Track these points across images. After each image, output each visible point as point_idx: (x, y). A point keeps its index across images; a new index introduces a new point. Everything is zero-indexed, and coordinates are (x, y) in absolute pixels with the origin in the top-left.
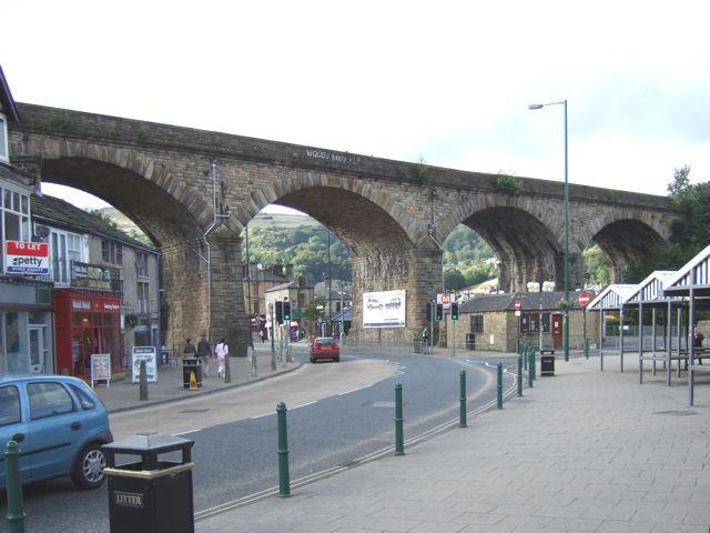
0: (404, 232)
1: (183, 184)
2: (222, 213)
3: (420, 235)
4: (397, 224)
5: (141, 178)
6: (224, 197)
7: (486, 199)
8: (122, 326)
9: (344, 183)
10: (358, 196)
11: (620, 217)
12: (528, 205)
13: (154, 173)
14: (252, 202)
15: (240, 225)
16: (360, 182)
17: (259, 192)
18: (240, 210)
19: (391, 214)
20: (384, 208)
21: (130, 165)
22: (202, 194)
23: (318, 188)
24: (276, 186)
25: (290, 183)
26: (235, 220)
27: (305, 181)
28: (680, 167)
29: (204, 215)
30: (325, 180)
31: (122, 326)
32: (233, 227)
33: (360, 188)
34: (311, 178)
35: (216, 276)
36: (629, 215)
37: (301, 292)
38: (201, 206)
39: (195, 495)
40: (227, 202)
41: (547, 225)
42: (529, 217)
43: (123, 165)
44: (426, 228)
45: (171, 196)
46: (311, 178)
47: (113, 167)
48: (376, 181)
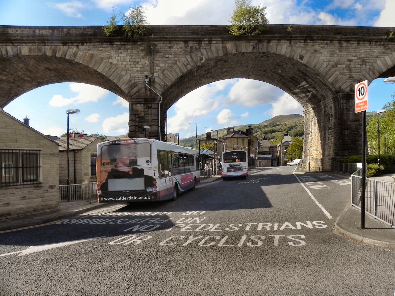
7: (225, 48)
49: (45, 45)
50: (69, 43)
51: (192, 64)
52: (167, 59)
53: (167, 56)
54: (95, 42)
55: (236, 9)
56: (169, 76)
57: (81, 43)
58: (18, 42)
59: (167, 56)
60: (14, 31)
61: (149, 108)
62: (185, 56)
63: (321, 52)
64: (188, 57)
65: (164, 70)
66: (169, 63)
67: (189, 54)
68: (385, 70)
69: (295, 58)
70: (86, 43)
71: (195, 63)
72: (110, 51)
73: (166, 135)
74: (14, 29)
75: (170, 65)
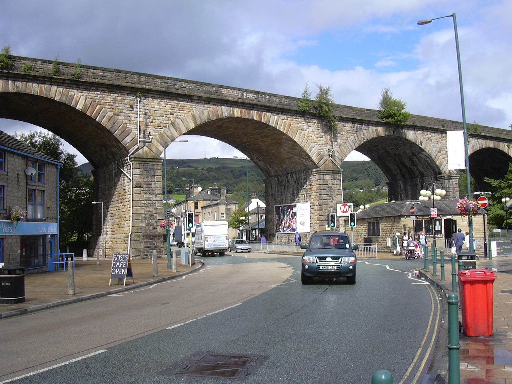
0: (307, 155)
1: (110, 114)
2: (144, 138)
3: (321, 157)
4: (301, 148)
5: (74, 109)
6: (147, 125)
7: (376, 130)
8: (110, 280)
9: (254, 115)
10: (266, 126)
11: (484, 147)
12: (411, 135)
13: (85, 105)
14: (172, 129)
15: (161, 148)
16: (268, 114)
17: (178, 121)
18: (161, 135)
19: (296, 140)
20: (289, 134)
21: (64, 99)
22: (128, 122)
23: (232, 120)
24: (194, 116)
25: (206, 114)
26: (156, 143)
27: (220, 113)
28: (387, 88)
29: (128, 139)
30: (237, 112)
31: (110, 280)
32: (154, 149)
33: (269, 119)
34: (225, 111)
35: (137, 190)
36: (491, 144)
37: (229, 206)
38: (126, 132)
39: (25, 281)
40: (149, 129)
41: (427, 151)
42: (412, 145)
43: (57, 99)
44: (326, 152)
45: (99, 124)
46: (225, 111)
47: (51, 101)
48: (282, 114)
49: (363, 125)
50: (272, 110)
51: (358, 142)
52: (342, 136)
53: (342, 133)
54: (172, 96)
55: (397, 100)
56: (344, 152)
57: (282, 112)
58: (152, 93)
59: (342, 133)
60: (226, 91)
61: (335, 180)
62: (353, 134)
63: (431, 140)
64: (355, 135)
65: (341, 145)
66: (343, 139)
67: (355, 133)
68: (485, 147)
69: (417, 144)
70: (285, 112)
71: (360, 141)
72: (302, 123)
73: (501, 142)
74: (226, 89)
75: (344, 141)
